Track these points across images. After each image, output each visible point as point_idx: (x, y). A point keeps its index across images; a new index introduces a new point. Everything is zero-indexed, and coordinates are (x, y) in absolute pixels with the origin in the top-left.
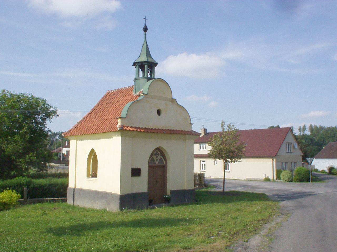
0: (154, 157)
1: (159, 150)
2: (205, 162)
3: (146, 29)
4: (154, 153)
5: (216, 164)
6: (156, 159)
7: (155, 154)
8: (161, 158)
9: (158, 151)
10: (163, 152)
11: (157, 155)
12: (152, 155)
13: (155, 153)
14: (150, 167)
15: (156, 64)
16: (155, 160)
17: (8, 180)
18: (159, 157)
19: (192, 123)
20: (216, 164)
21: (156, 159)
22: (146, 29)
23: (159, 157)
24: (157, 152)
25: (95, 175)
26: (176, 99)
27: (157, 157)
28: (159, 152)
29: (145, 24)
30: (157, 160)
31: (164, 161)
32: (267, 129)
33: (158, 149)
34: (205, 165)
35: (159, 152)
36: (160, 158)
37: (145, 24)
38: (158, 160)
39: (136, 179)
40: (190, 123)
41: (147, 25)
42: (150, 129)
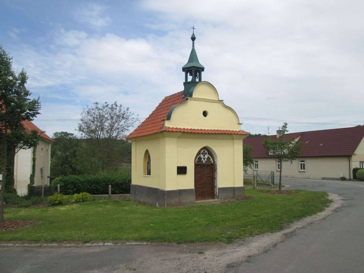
0: (202, 156)
1: (206, 150)
2: (304, 161)
3: (193, 39)
4: (201, 152)
5: (292, 163)
6: (203, 158)
7: (202, 154)
8: (208, 157)
9: (205, 150)
10: (212, 152)
11: (204, 154)
12: (199, 153)
13: (202, 151)
14: (196, 165)
15: (203, 69)
16: (203, 159)
17: (254, 135)
18: (206, 156)
19: (240, 123)
20: (292, 163)
21: (203, 158)
22: (193, 39)
23: (206, 156)
24: (204, 151)
25: (149, 173)
26: (223, 101)
27: (204, 156)
28: (207, 150)
29: (193, 34)
30: (204, 159)
31: (211, 159)
32: (274, 137)
33: (205, 148)
34: (257, 164)
35: (206, 152)
36: (207, 157)
37: (193, 34)
38: (206, 159)
39: (182, 177)
40: (238, 123)
41: (195, 34)
42: (195, 129)
